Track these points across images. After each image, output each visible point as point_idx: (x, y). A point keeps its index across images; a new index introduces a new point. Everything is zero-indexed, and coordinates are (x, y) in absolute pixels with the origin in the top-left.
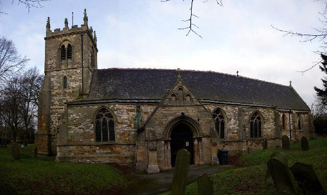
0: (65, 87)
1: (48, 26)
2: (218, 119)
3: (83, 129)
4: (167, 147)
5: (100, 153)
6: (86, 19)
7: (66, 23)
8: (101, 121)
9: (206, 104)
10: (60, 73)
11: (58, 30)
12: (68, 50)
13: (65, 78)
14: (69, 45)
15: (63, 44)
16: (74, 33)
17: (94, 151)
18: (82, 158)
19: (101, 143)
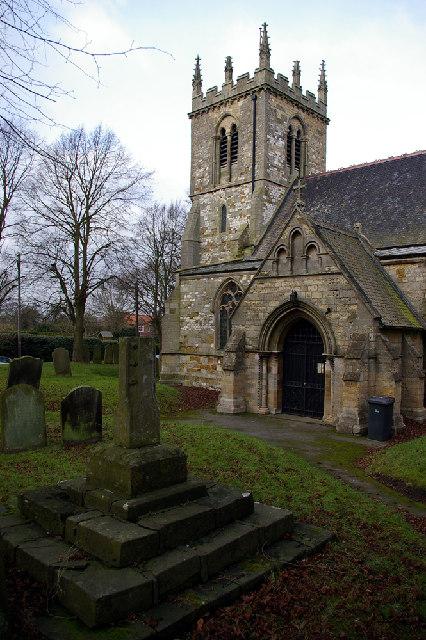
0: (223, 229)
1: (197, 81)
4: (269, 370)
6: (265, 51)
9: (389, 264)
12: (233, 139)
15: (222, 125)
18: (197, 379)
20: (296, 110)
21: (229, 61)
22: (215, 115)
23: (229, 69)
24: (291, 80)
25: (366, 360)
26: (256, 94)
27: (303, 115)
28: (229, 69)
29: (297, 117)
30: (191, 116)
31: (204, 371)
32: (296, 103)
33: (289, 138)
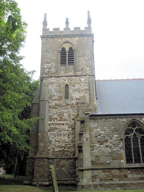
1: (45, 23)
2: (135, 135)
3: (111, 147)
5: (134, 179)
6: (89, 22)
7: (67, 23)
8: (131, 137)
10: (61, 80)
11: (57, 29)
13: (67, 86)
14: (71, 49)
16: (53, 100)
17: (61, 145)
19: (133, 165)
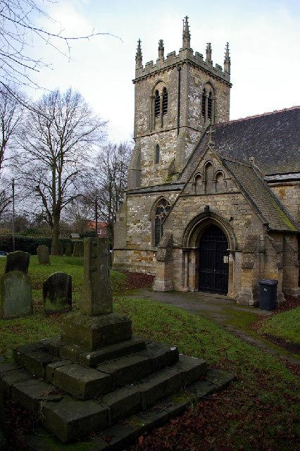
0: (157, 162)
1: (139, 57)
4: (189, 261)
6: (187, 36)
9: (274, 186)
12: (164, 98)
15: (156, 88)
18: (139, 267)
20: (208, 78)
21: (161, 43)
22: (151, 81)
23: (161, 49)
24: (205, 56)
25: (258, 254)
26: (181, 66)
27: (213, 81)
28: (161, 49)
29: (209, 83)
30: (134, 82)
31: (143, 262)
32: (209, 73)
33: (204, 97)
